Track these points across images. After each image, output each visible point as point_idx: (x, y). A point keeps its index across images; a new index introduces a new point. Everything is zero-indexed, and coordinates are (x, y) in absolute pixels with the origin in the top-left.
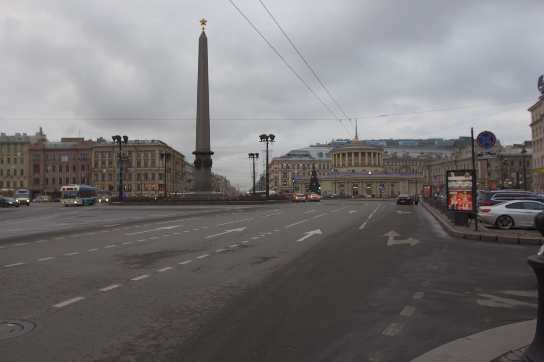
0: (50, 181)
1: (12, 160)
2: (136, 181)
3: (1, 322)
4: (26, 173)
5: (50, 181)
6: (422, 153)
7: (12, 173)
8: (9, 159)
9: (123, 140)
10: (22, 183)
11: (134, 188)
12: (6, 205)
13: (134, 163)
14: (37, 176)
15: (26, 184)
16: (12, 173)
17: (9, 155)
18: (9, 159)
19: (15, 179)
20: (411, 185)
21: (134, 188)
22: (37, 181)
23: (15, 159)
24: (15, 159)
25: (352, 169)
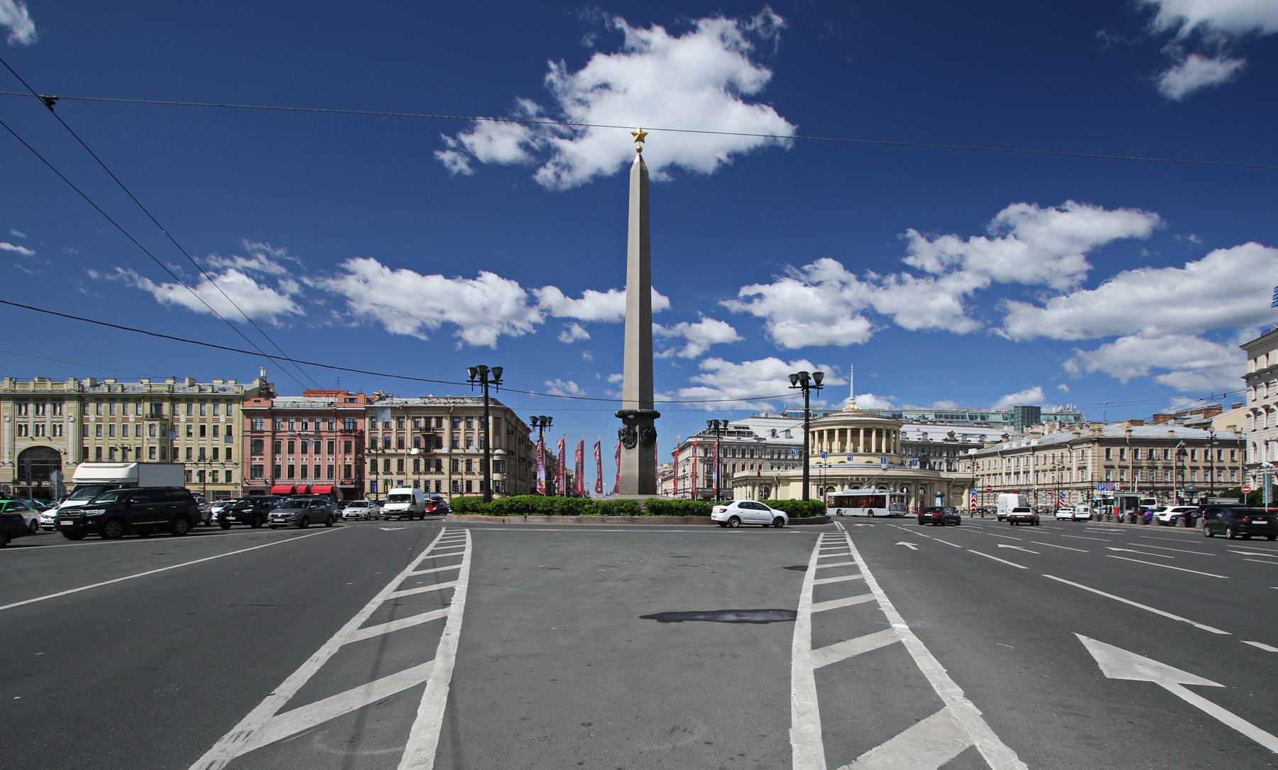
0: (285, 472)
1: (209, 430)
2: (450, 474)
3: (6, 386)
4: (236, 456)
5: (285, 472)
6: (951, 434)
7: (209, 454)
8: (203, 428)
9: (812, 382)
10: (229, 473)
11: (445, 487)
12: (181, 525)
13: (182, 430)
14: (257, 462)
15: (236, 477)
16: (209, 454)
17: (113, 420)
18: (203, 428)
19: (216, 466)
20: (952, 491)
21: (445, 487)
22: (257, 471)
23: (216, 427)
24: (216, 427)
25: (869, 458)
